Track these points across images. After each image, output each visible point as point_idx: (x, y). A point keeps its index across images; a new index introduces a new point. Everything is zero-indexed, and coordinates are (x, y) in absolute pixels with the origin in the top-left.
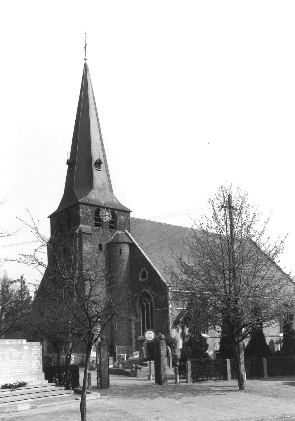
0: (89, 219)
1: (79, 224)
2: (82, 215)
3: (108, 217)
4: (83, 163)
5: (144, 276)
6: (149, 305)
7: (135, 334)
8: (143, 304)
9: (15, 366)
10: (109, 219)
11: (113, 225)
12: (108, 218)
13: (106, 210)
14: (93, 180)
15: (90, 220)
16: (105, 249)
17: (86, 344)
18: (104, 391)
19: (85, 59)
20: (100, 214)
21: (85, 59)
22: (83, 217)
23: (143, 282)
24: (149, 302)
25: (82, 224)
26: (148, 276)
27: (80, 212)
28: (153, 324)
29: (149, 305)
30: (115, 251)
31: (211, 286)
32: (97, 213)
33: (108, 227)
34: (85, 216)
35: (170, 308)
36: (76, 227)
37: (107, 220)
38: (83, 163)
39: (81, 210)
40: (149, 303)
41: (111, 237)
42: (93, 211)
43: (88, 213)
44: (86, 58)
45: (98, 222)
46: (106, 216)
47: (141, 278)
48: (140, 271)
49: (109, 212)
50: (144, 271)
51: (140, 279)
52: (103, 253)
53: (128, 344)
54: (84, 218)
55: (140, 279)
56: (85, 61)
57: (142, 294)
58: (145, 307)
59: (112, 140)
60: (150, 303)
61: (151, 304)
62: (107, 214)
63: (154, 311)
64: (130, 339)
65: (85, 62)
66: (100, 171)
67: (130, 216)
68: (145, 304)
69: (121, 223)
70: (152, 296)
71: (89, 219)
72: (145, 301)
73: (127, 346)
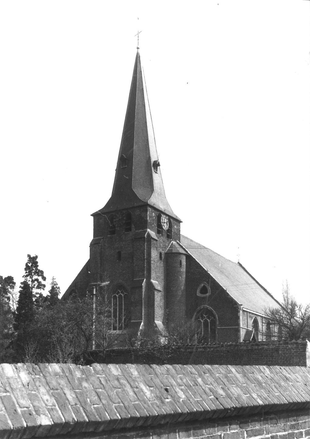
1: (147, 228)
2: (129, 221)
4: (134, 162)
9: (264, 393)
14: (153, 182)
16: (164, 259)
18: (295, 420)
19: (138, 48)
21: (138, 48)
27: (148, 215)
29: (208, 322)
31: (54, 306)
32: (159, 218)
35: (241, 326)
36: (140, 231)
38: (134, 162)
39: (148, 213)
44: (138, 47)
47: (200, 294)
48: (198, 286)
51: (198, 294)
52: (162, 263)
55: (198, 294)
56: (137, 50)
59: (161, 143)
63: (218, 328)
65: (138, 51)
66: (157, 173)
70: (216, 313)
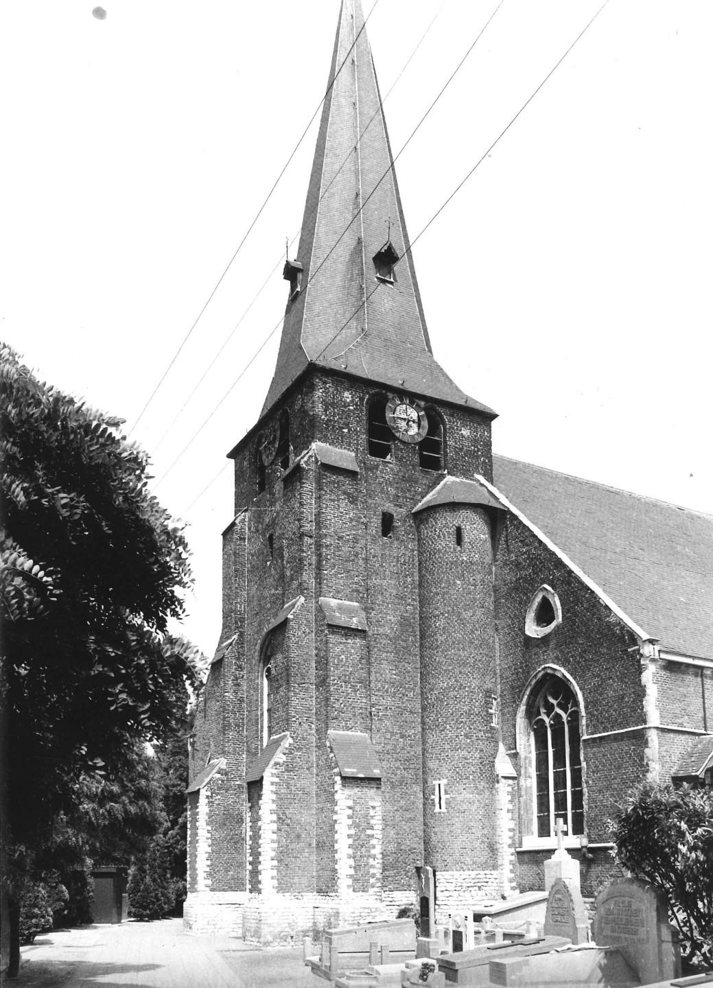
0: (347, 425)
3: (415, 426)
5: (545, 614)
6: (565, 720)
7: (510, 830)
8: (542, 721)
10: (418, 434)
11: (430, 456)
12: (416, 430)
13: (408, 402)
15: (350, 430)
17: (394, 272)
20: (389, 415)
22: (326, 415)
23: (545, 640)
24: (565, 710)
25: (324, 439)
26: (559, 619)
28: (581, 793)
30: (439, 536)
33: (416, 459)
34: (334, 416)
37: (412, 437)
40: (564, 716)
41: (427, 493)
42: (362, 399)
43: (346, 405)
45: (380, 438)
46: (407, 421)
49: (418, 408)
50: (545, 600)
51: (533, 630)
53: (484, 866)
54: (329, 420)
57: (540, 684)
58: (560, 812)
60: (570, 715)
61: (575, 717)
62: (414, 414)
64: (493, 849)
67: (496, 450)
68: (547, 720)
69: (461, 449)
71: (347, 425)
72: (550, 708)
73: (482, 872)
